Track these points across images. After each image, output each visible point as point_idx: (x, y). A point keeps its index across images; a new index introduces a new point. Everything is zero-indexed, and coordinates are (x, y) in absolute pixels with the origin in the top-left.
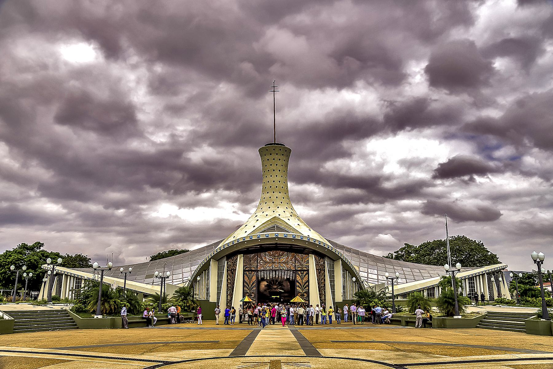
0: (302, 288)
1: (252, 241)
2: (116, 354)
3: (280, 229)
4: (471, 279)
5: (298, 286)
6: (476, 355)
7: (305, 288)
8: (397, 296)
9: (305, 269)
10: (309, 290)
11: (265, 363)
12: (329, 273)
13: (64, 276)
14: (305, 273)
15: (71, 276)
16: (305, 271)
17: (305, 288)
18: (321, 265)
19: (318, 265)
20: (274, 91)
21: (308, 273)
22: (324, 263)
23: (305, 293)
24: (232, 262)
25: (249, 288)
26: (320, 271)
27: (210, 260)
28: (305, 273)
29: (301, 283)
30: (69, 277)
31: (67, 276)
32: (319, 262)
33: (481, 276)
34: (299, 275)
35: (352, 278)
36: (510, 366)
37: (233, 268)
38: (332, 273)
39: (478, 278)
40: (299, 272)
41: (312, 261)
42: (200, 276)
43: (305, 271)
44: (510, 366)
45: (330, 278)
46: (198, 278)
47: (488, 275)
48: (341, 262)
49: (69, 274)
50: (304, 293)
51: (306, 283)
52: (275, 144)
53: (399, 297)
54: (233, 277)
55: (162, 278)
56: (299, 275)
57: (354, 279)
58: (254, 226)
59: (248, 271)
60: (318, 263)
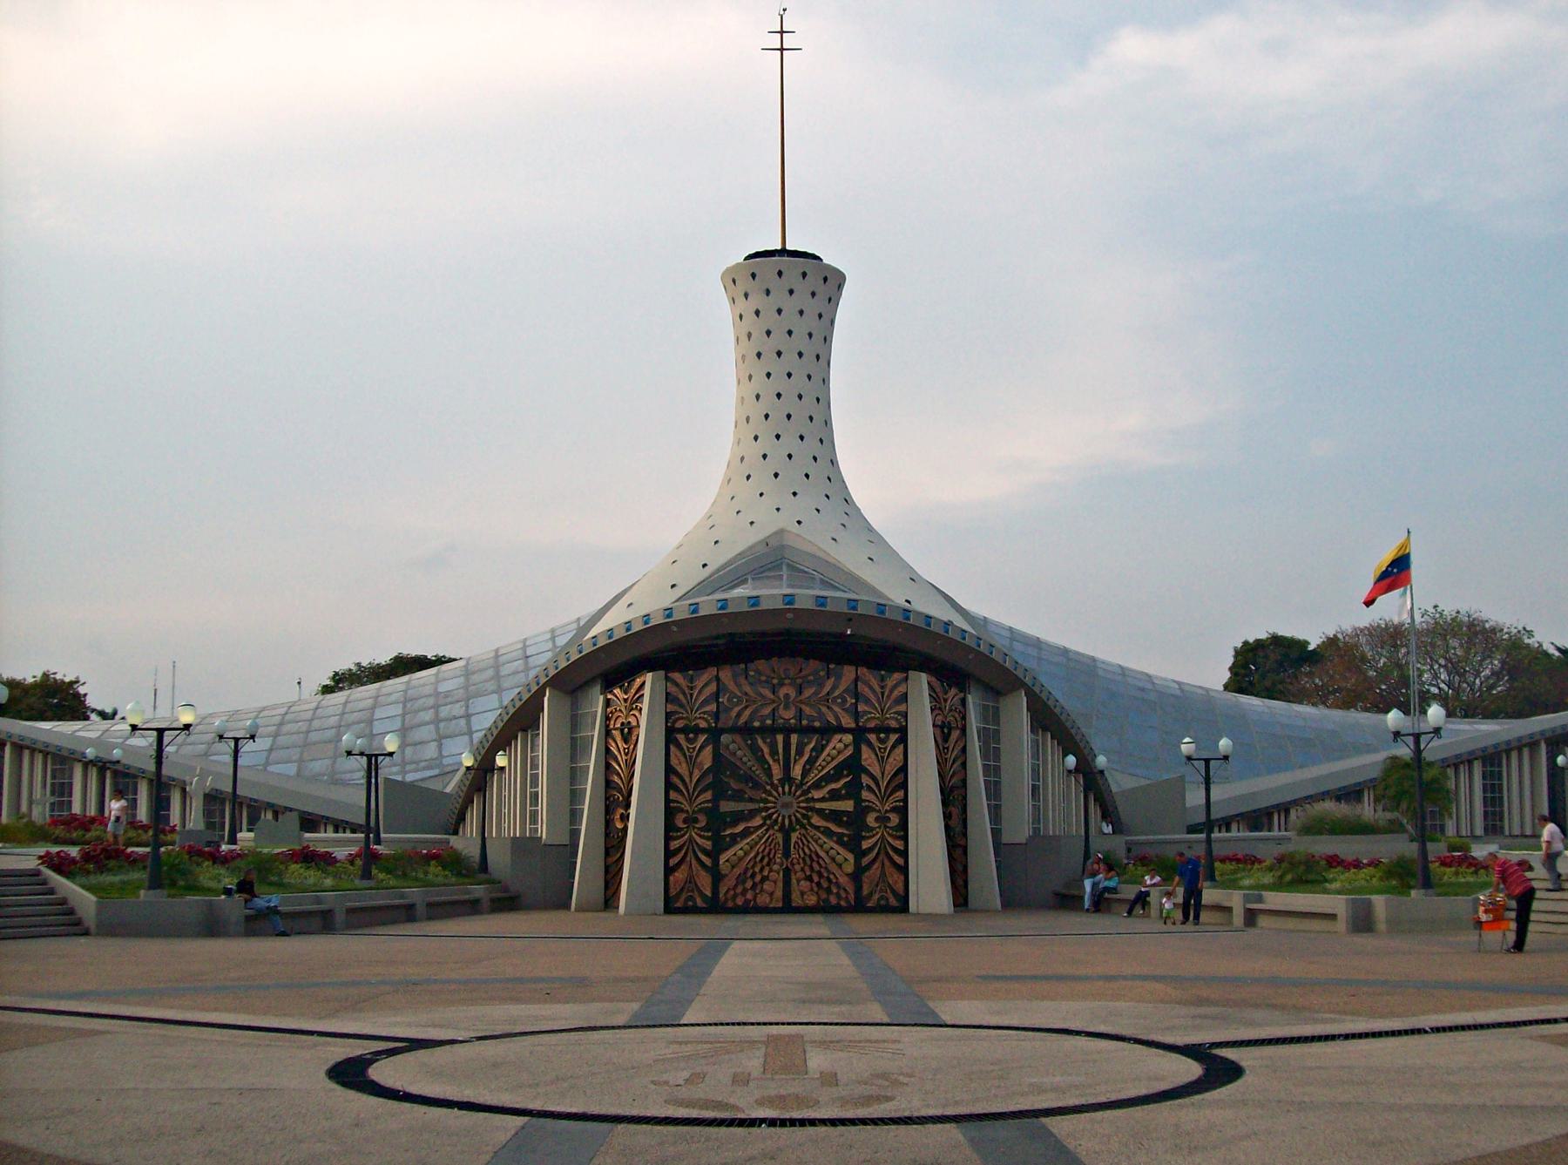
0: (880, 790)
1: (696, 622)
2: (626, 888)
3: (799, 573)
4: (1492, 759)
5: (869, 788)
6: (1453, 1009)
7: (680, 849)
8: (1226, 824)
9: (893, 724)
10: (905, 800)
11: (752, 1043)
12: (979, 738)
13: (8, 749)
14: (894, 737)
15: (33, 751)
16: (895, 730)
17: (704, 703)
18: (951, 710)
19: (940, 709)
20: (782, 49)
21: (903, 740)
22: (963, 702)
23: (894, 810)
24: (625, 700)
25: (688, 791)
26: (948, 732)
27: (540, 694)
28: (894, 737)
29: (878, 775)
30: (26, 753)
31: (19, 748)
32: (946, 700)
33: (1526, 752)
34: (870, 744)
35: (1065, 755)
36: (1543, 1038)
37: (629, 722)
38: (991, 740)
39: (1514, 755)
40: (872, 737)
41: (920, 685)
42: (505, 751)
43: (895, 730)
44: (1543, 1038)
45: (985, 756)
46: (501, 761)
47: (1550, 748)
48: (1025, 699)
49: (27, 743)
50: (887, 811)
51: (895, 775)
52: (783, 252)
53: (1234, 826)
54: (626, 754)
55: (369, 757)
56: (870, 744)
57: (1071, 760)
58: (705, 565)
59: (681, 731)
60: (940, 703)
